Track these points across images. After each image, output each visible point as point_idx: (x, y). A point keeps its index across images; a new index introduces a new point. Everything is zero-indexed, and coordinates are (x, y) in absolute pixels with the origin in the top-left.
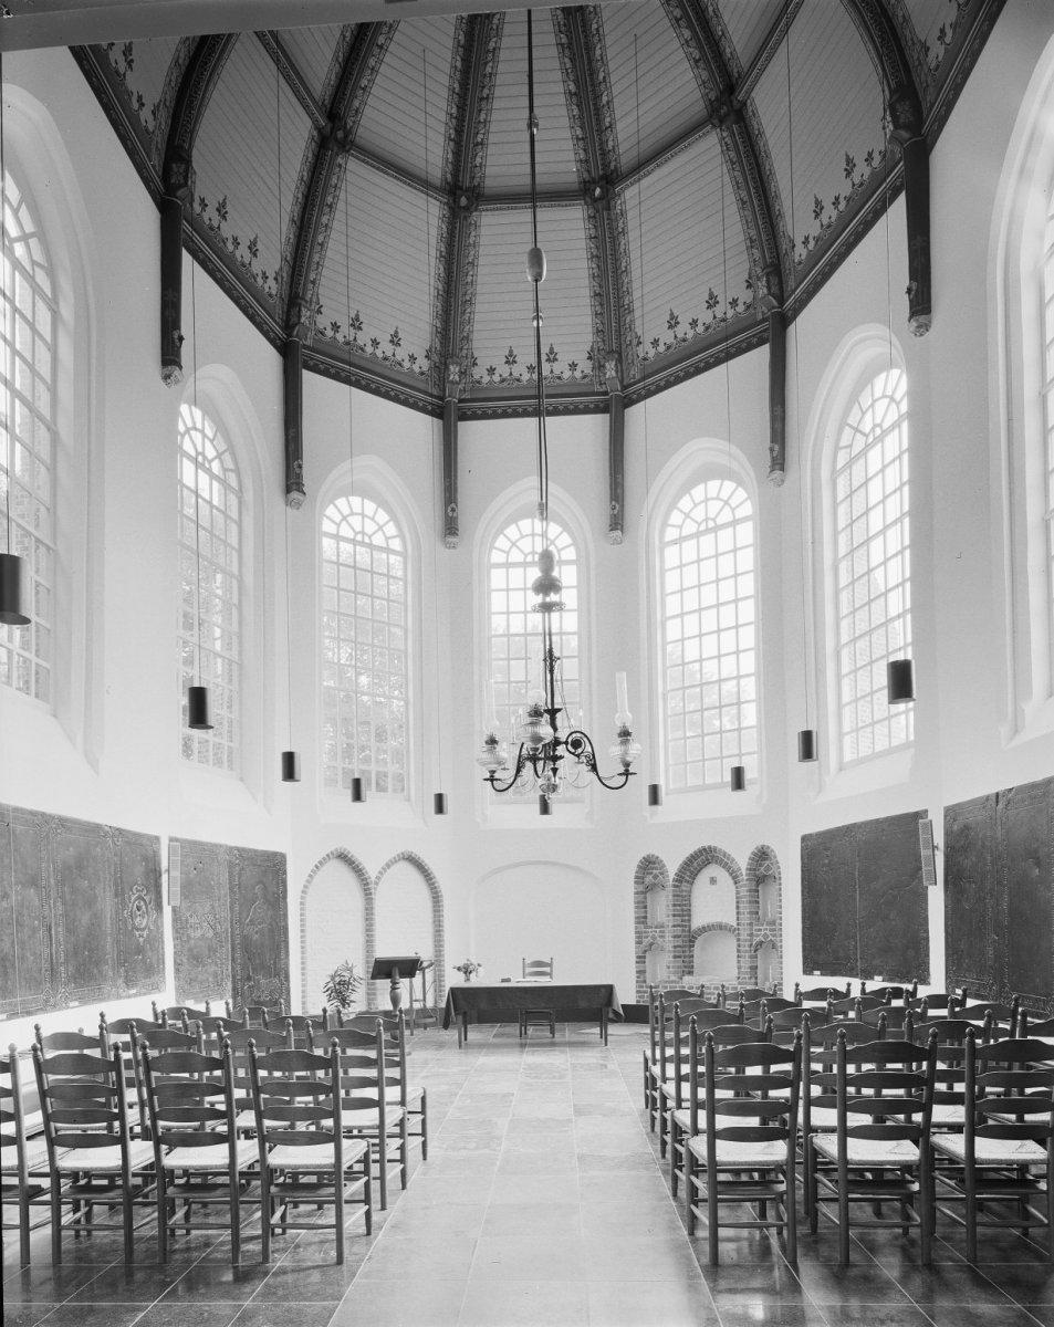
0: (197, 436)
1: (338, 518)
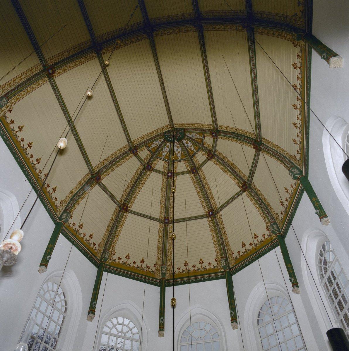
1: (111, 326)
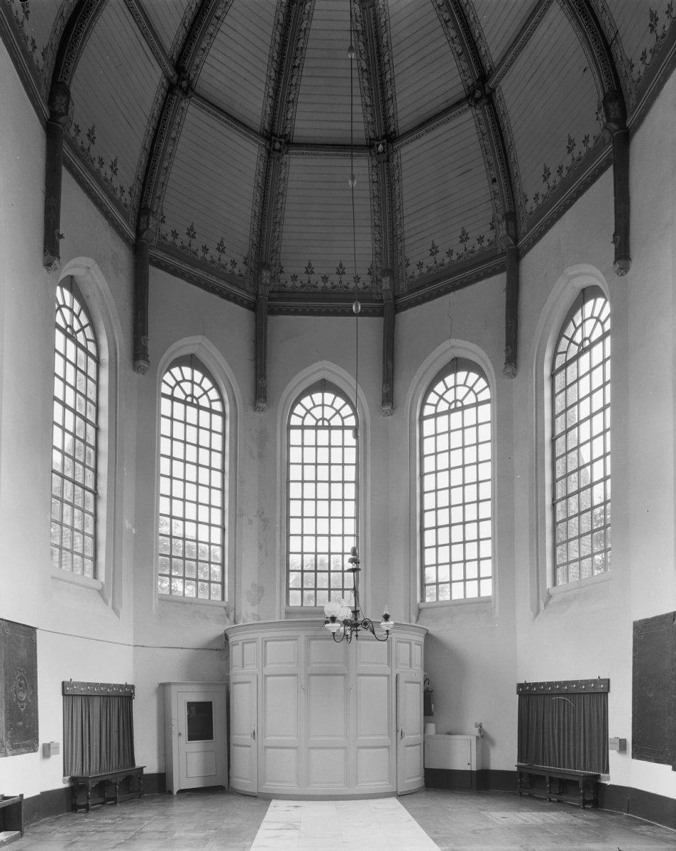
0: (66, 312)
1: (173, 383)
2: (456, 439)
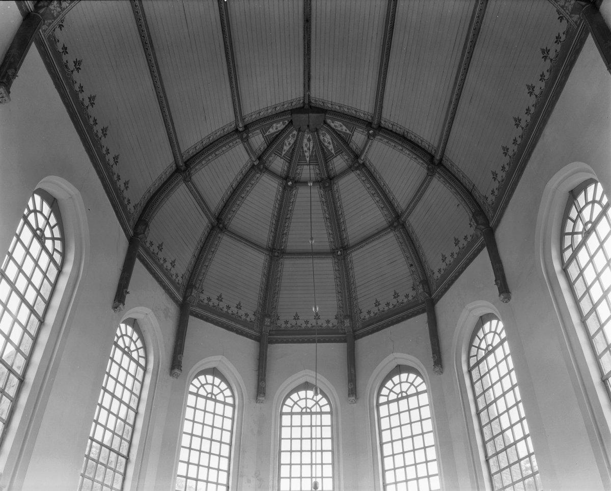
2: (405, 418)
